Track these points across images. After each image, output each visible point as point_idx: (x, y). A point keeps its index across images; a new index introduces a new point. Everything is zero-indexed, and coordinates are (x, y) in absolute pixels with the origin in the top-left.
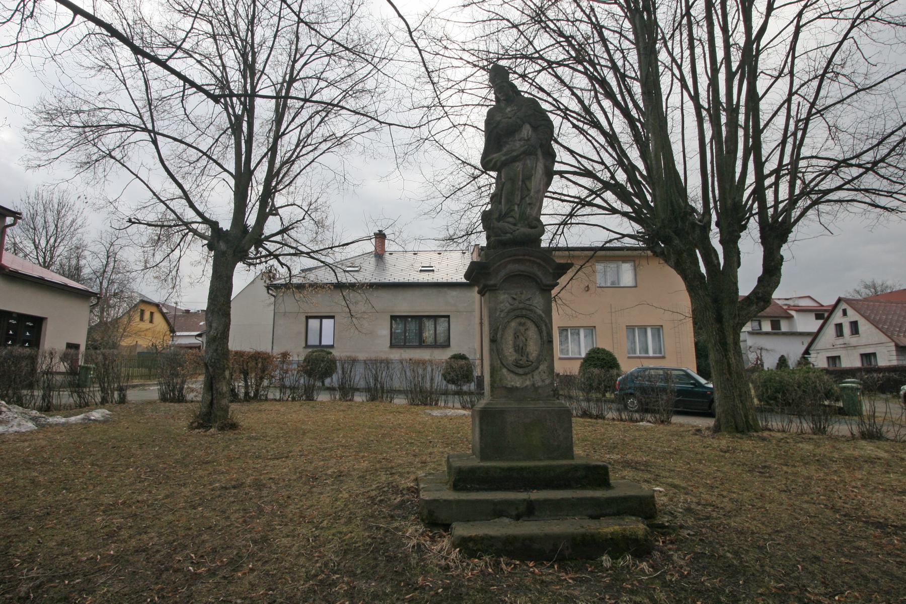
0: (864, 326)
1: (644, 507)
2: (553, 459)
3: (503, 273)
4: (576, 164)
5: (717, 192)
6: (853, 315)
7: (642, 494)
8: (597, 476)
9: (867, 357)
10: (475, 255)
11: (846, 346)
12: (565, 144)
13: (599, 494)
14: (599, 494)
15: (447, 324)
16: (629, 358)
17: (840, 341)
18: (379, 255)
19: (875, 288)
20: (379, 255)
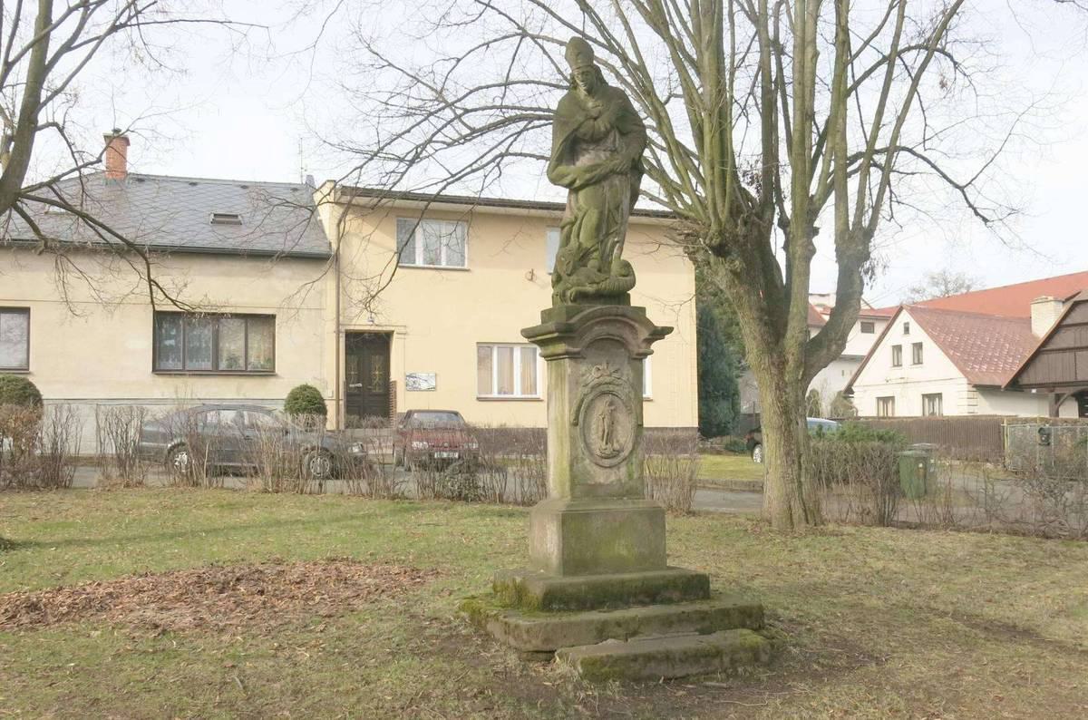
0: (931, 350)
1: (752, 617)
2: (645, 570)
3: (588, 338)
4: (741, 49)
5: (780, 104)
6: (918, 334)
7: (746, 604)
8: (697, 586)
9: (932, 398)
10: (840, 321)
11: (904, 382)
12: (465, 53)
13: (704, 606)
14: (704, 606)
15: (25, 324)
16: (479, 399)
17: (898, 372)
18: (843, 372)
19: (19, 264)
20: (843, 372)
